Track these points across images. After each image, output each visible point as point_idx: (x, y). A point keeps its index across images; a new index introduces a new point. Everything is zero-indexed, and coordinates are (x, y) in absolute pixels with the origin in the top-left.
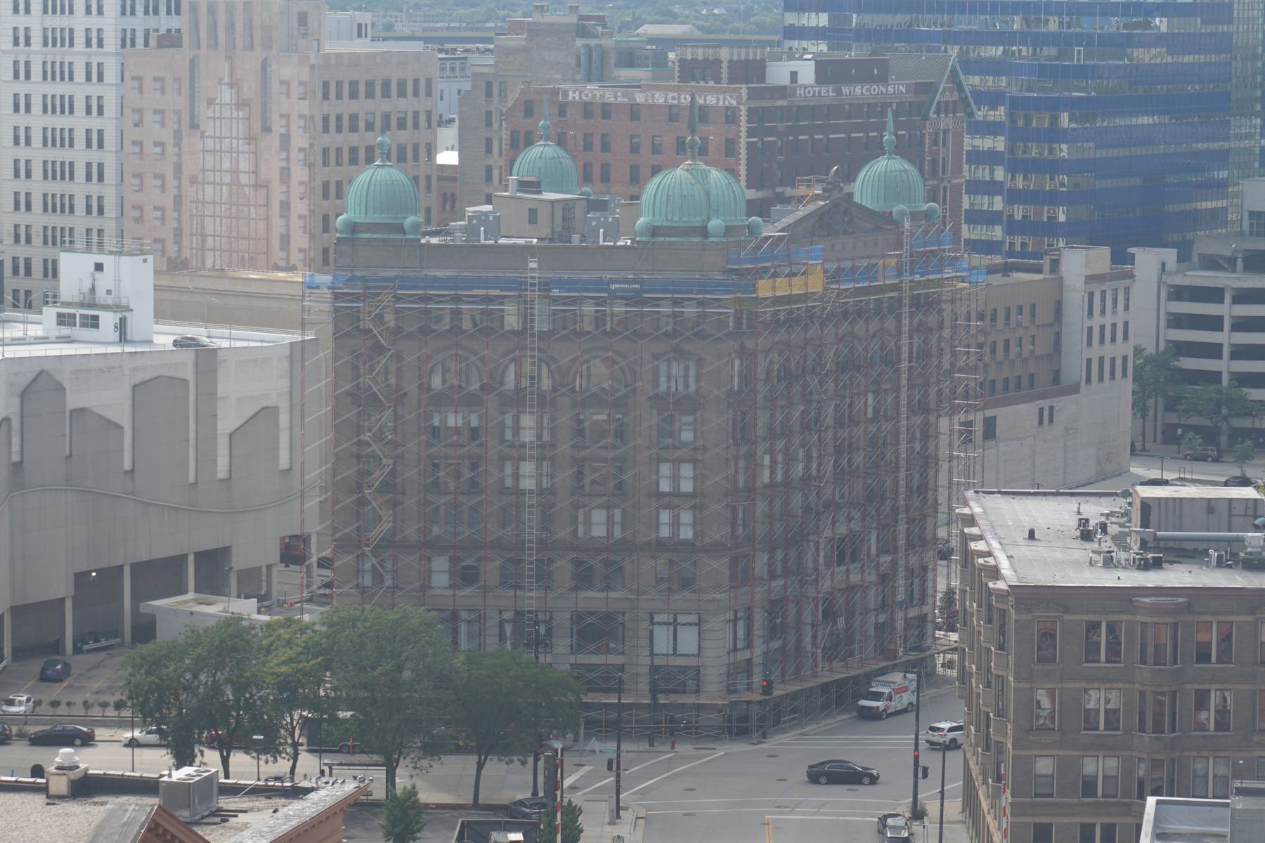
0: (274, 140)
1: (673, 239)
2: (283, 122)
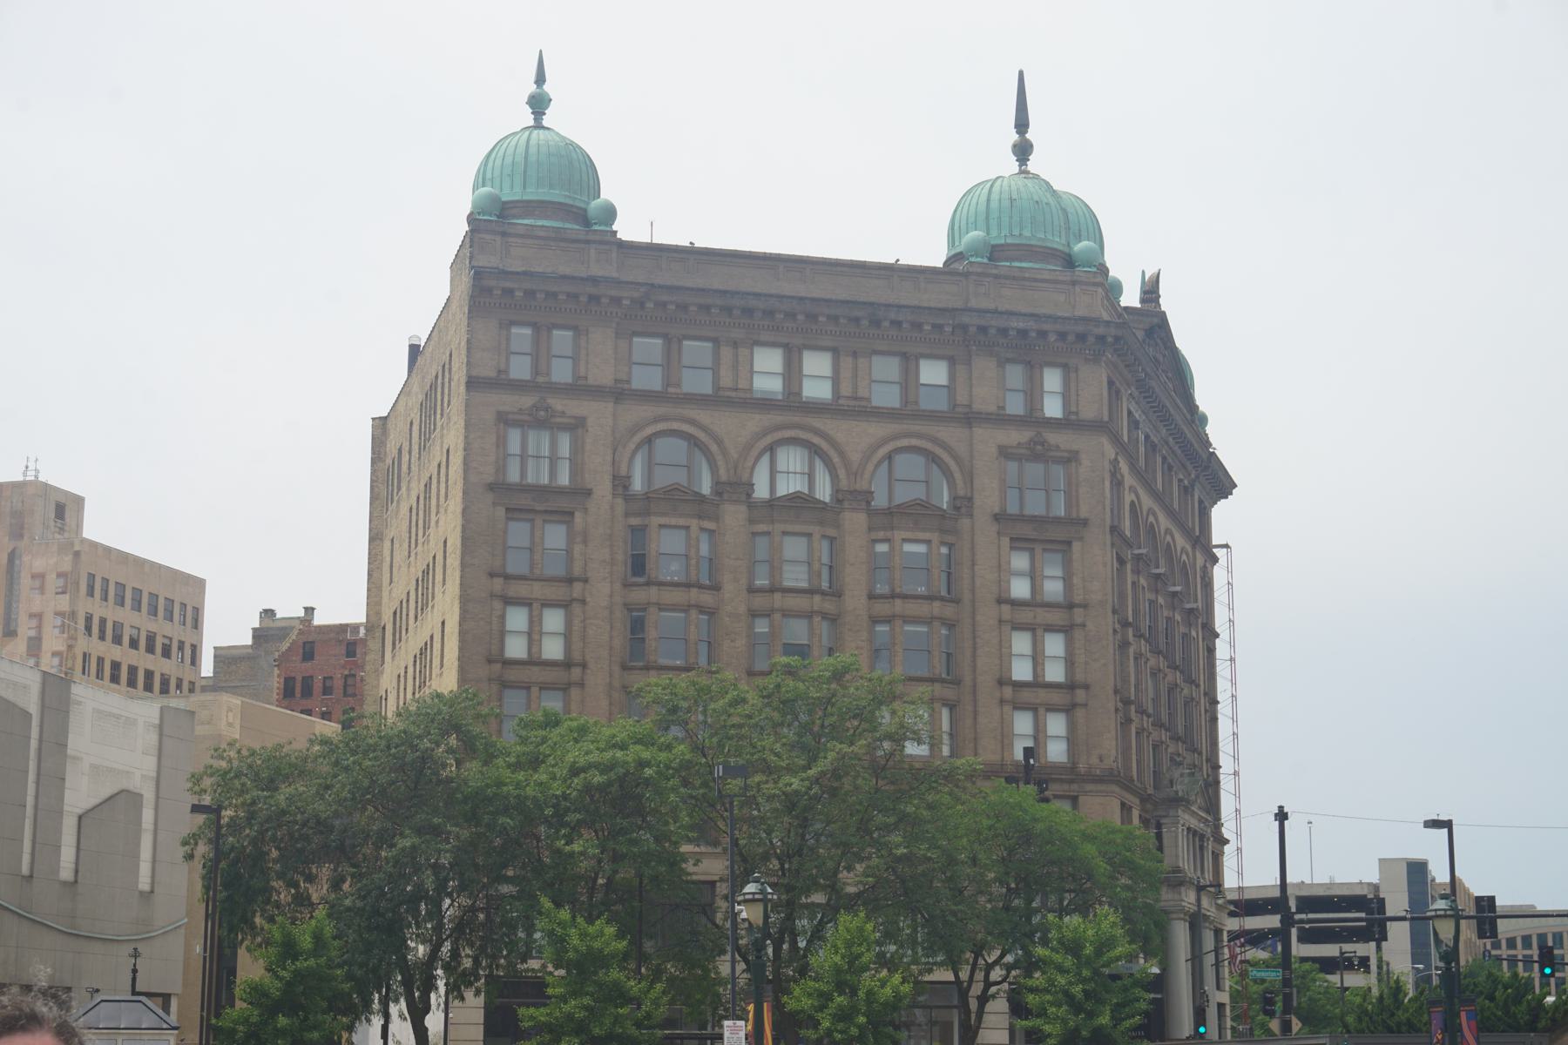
1: (1024, 265)
2: (34, 623)
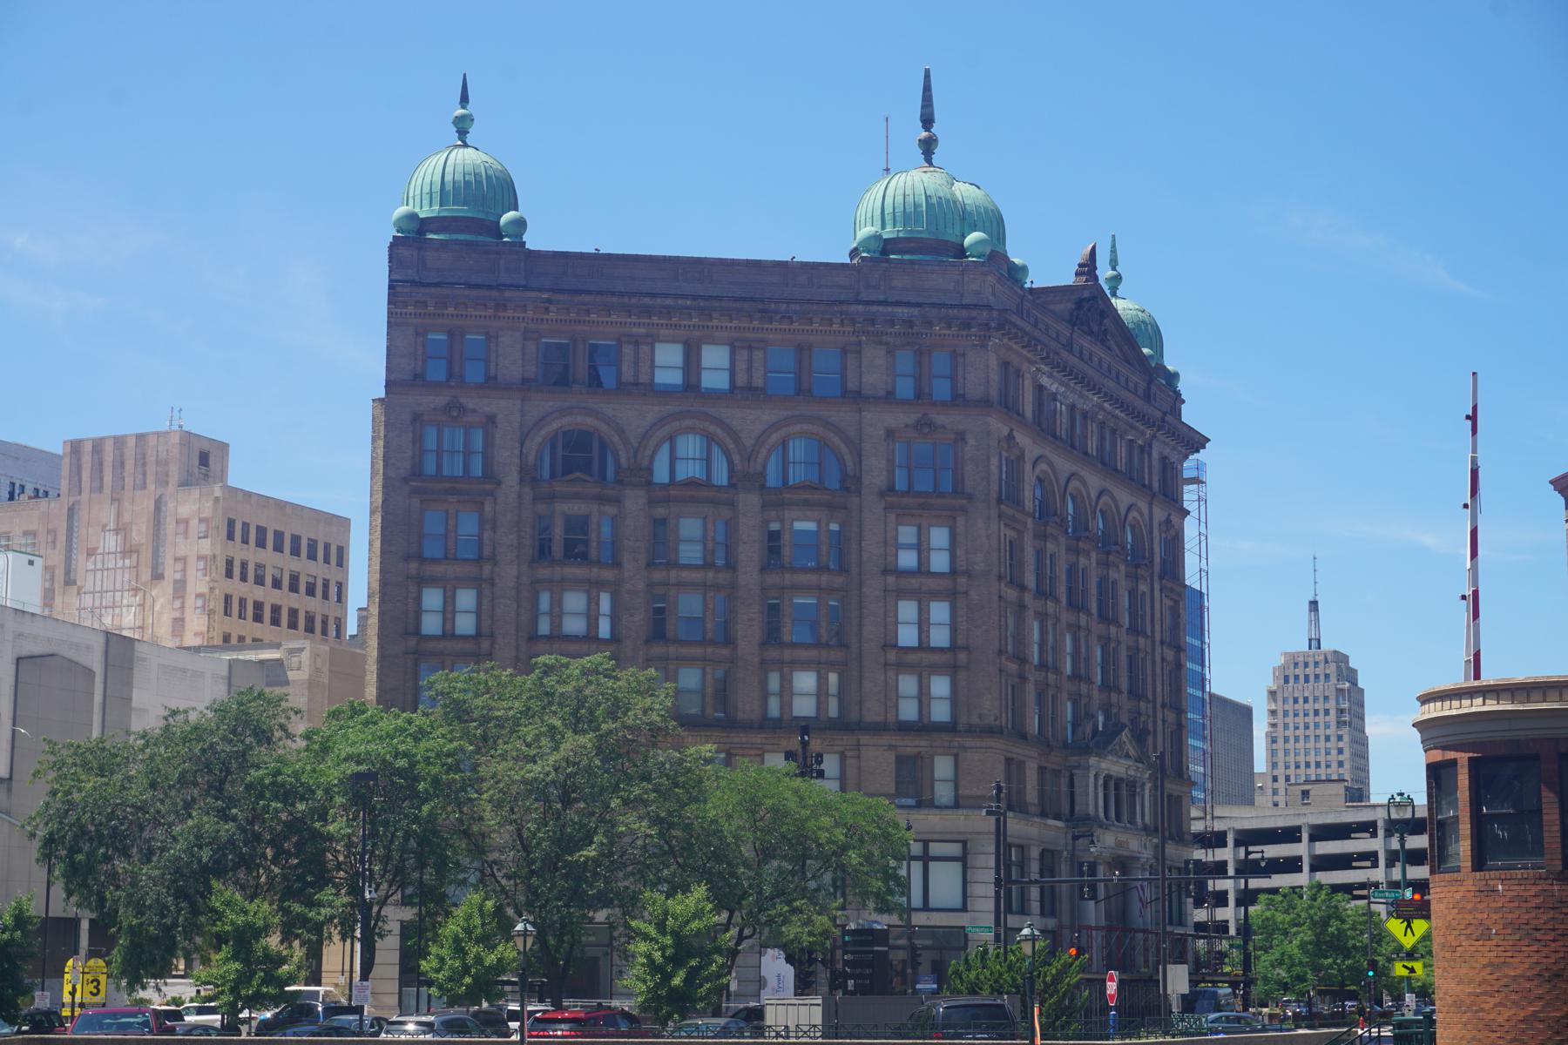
0: (167, 587)
2: (179, 566)
